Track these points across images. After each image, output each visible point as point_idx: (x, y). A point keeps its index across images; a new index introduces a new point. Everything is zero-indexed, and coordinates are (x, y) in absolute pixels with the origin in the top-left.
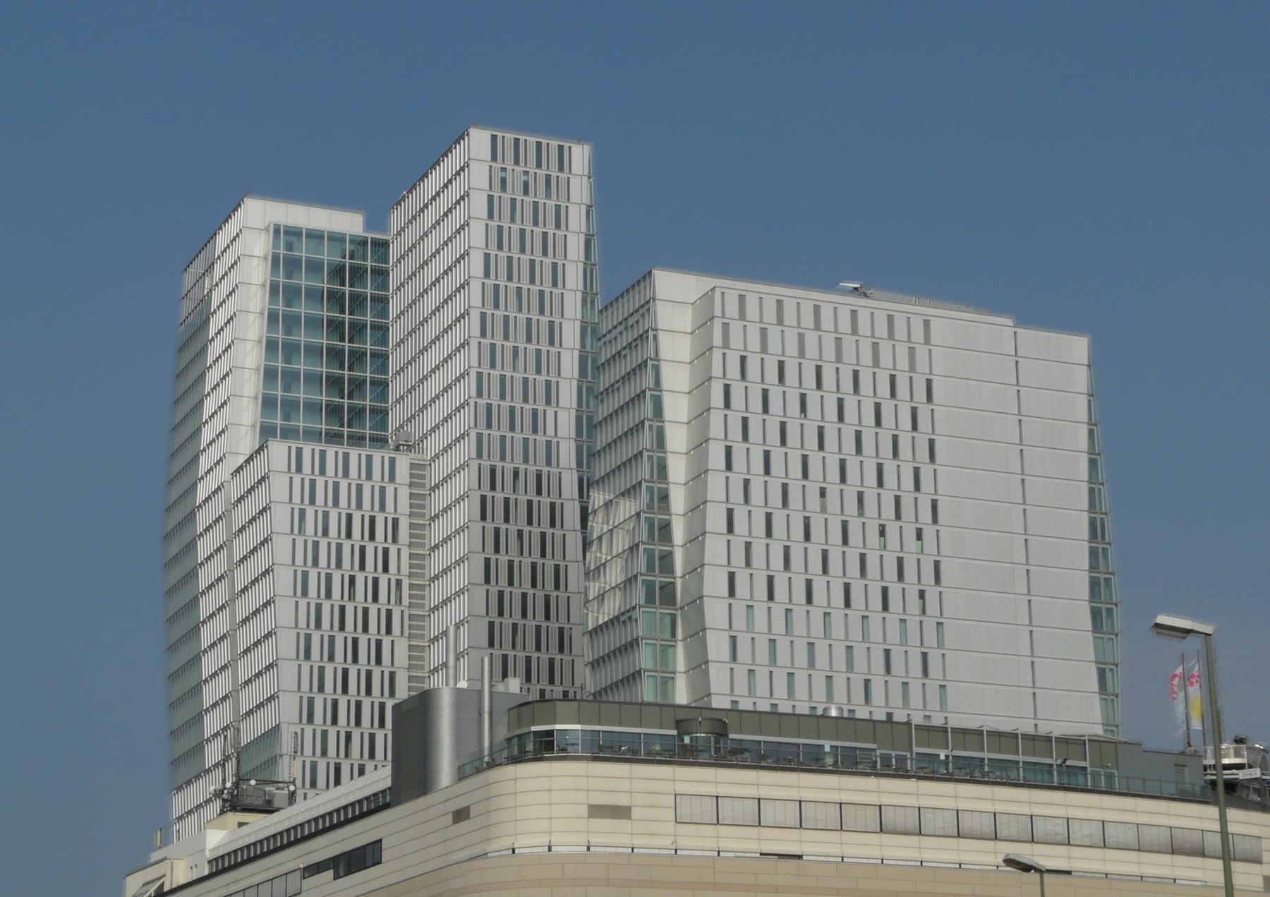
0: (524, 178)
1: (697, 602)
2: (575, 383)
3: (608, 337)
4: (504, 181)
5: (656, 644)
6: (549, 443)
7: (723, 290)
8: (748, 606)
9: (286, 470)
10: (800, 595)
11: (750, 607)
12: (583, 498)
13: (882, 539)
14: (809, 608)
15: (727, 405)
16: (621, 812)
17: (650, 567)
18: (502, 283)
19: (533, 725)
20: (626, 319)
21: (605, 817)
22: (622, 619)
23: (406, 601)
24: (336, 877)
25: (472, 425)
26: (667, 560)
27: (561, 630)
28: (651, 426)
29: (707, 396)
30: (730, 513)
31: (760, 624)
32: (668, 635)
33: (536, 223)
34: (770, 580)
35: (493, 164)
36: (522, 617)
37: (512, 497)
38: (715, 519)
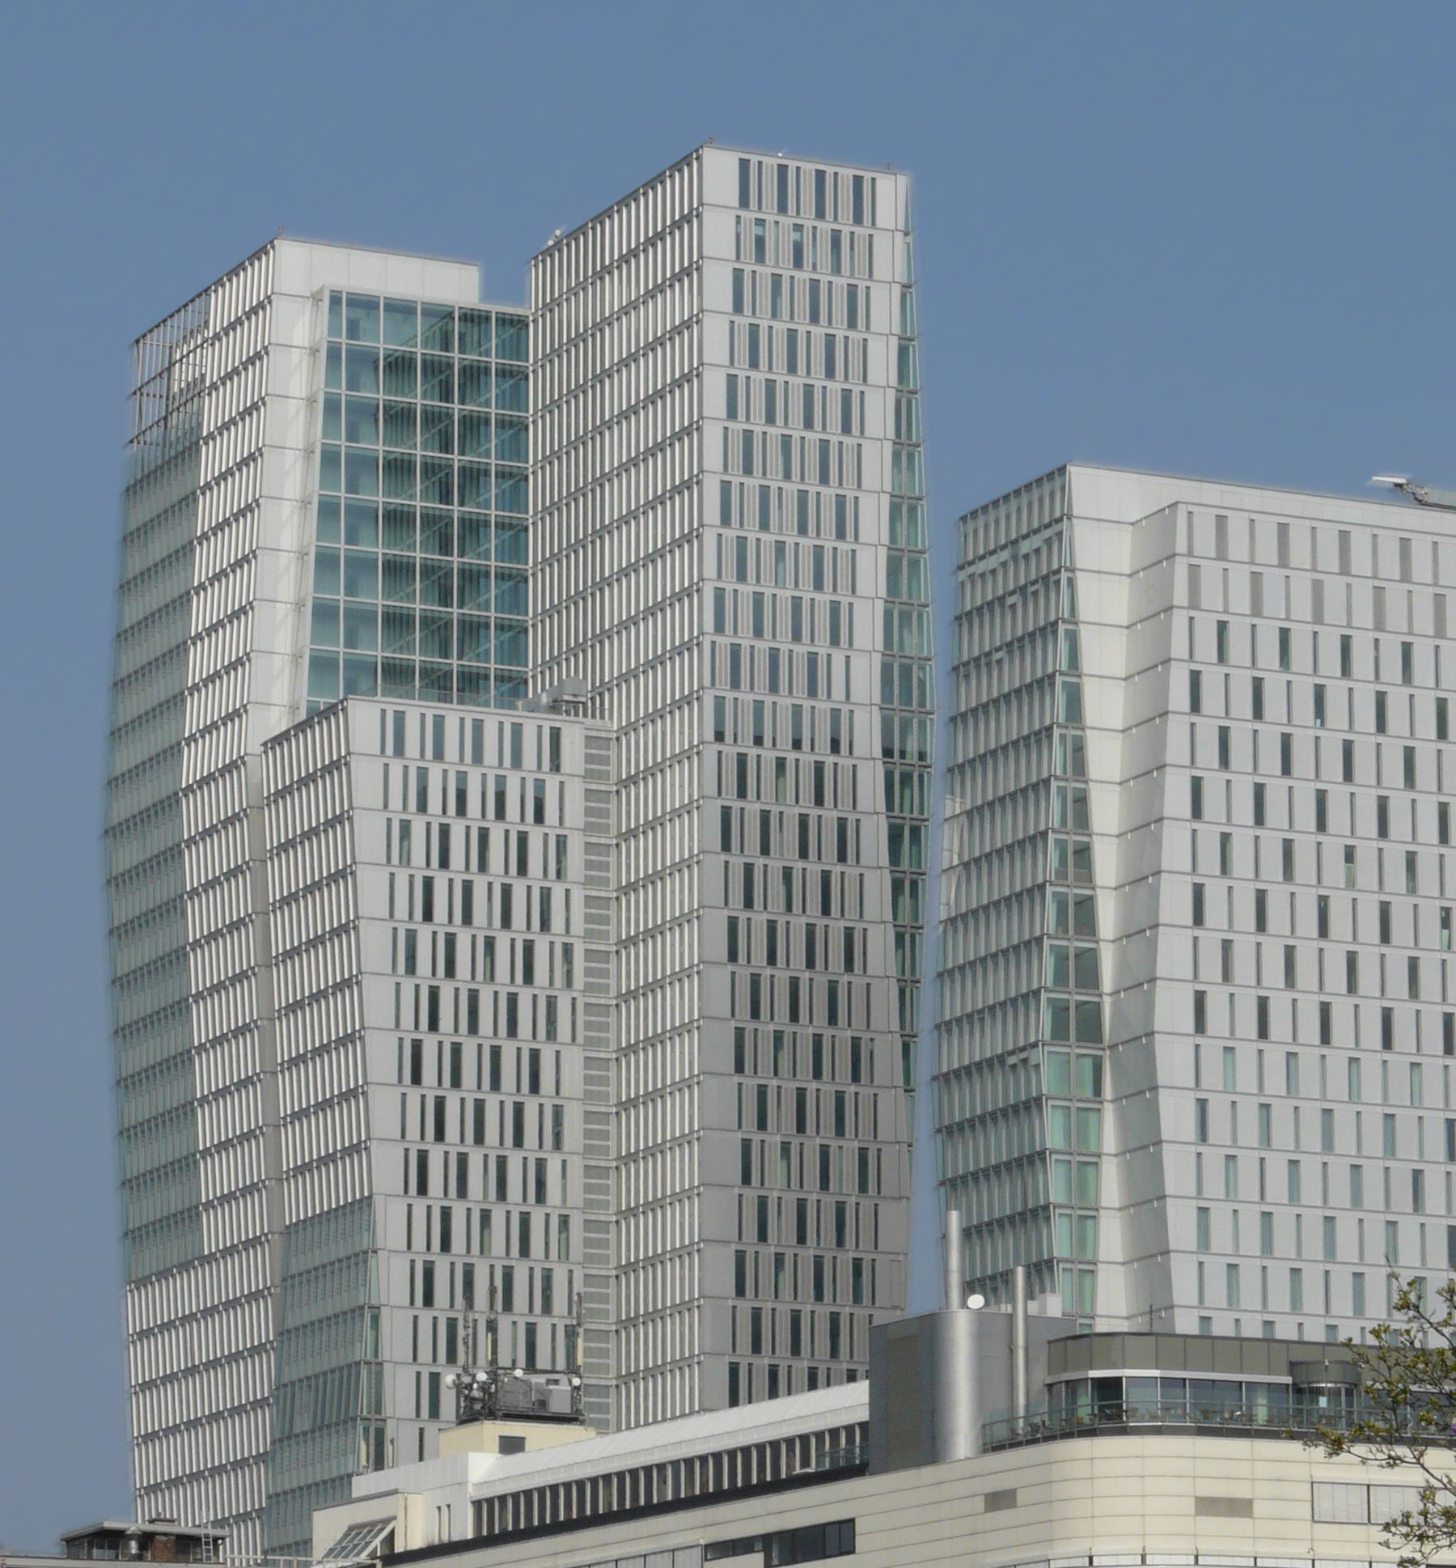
0: (794, 236)
2: (880, 606)
3: (981, 567)
4: (760, 242)
5: (1069, 1108)
6: (836, 714)
7: (1191, 508)
8: (1225, 1048)
10: (1310, 1029)
12: (893, 811)
13: (1446, 932)
14: (1325, 1051)
15: (1195, 706)
16: (1239, 1507)
17: (1061, 977)
18: (758, 428)
20: (1015, 542)
21: (1218, 1514)
22: (1012, 1060)
23: (579, 980)
25: (707, 682)
26: (1088, 973)
28: (1063, 737)
29: (1162, 690)
30: (1198, 892)
32: (1088, 1092)
34: (1263, 1005)
35: (743, 214)
36: (791, 1021)
37: (775, 810)
38: (1175, 902)
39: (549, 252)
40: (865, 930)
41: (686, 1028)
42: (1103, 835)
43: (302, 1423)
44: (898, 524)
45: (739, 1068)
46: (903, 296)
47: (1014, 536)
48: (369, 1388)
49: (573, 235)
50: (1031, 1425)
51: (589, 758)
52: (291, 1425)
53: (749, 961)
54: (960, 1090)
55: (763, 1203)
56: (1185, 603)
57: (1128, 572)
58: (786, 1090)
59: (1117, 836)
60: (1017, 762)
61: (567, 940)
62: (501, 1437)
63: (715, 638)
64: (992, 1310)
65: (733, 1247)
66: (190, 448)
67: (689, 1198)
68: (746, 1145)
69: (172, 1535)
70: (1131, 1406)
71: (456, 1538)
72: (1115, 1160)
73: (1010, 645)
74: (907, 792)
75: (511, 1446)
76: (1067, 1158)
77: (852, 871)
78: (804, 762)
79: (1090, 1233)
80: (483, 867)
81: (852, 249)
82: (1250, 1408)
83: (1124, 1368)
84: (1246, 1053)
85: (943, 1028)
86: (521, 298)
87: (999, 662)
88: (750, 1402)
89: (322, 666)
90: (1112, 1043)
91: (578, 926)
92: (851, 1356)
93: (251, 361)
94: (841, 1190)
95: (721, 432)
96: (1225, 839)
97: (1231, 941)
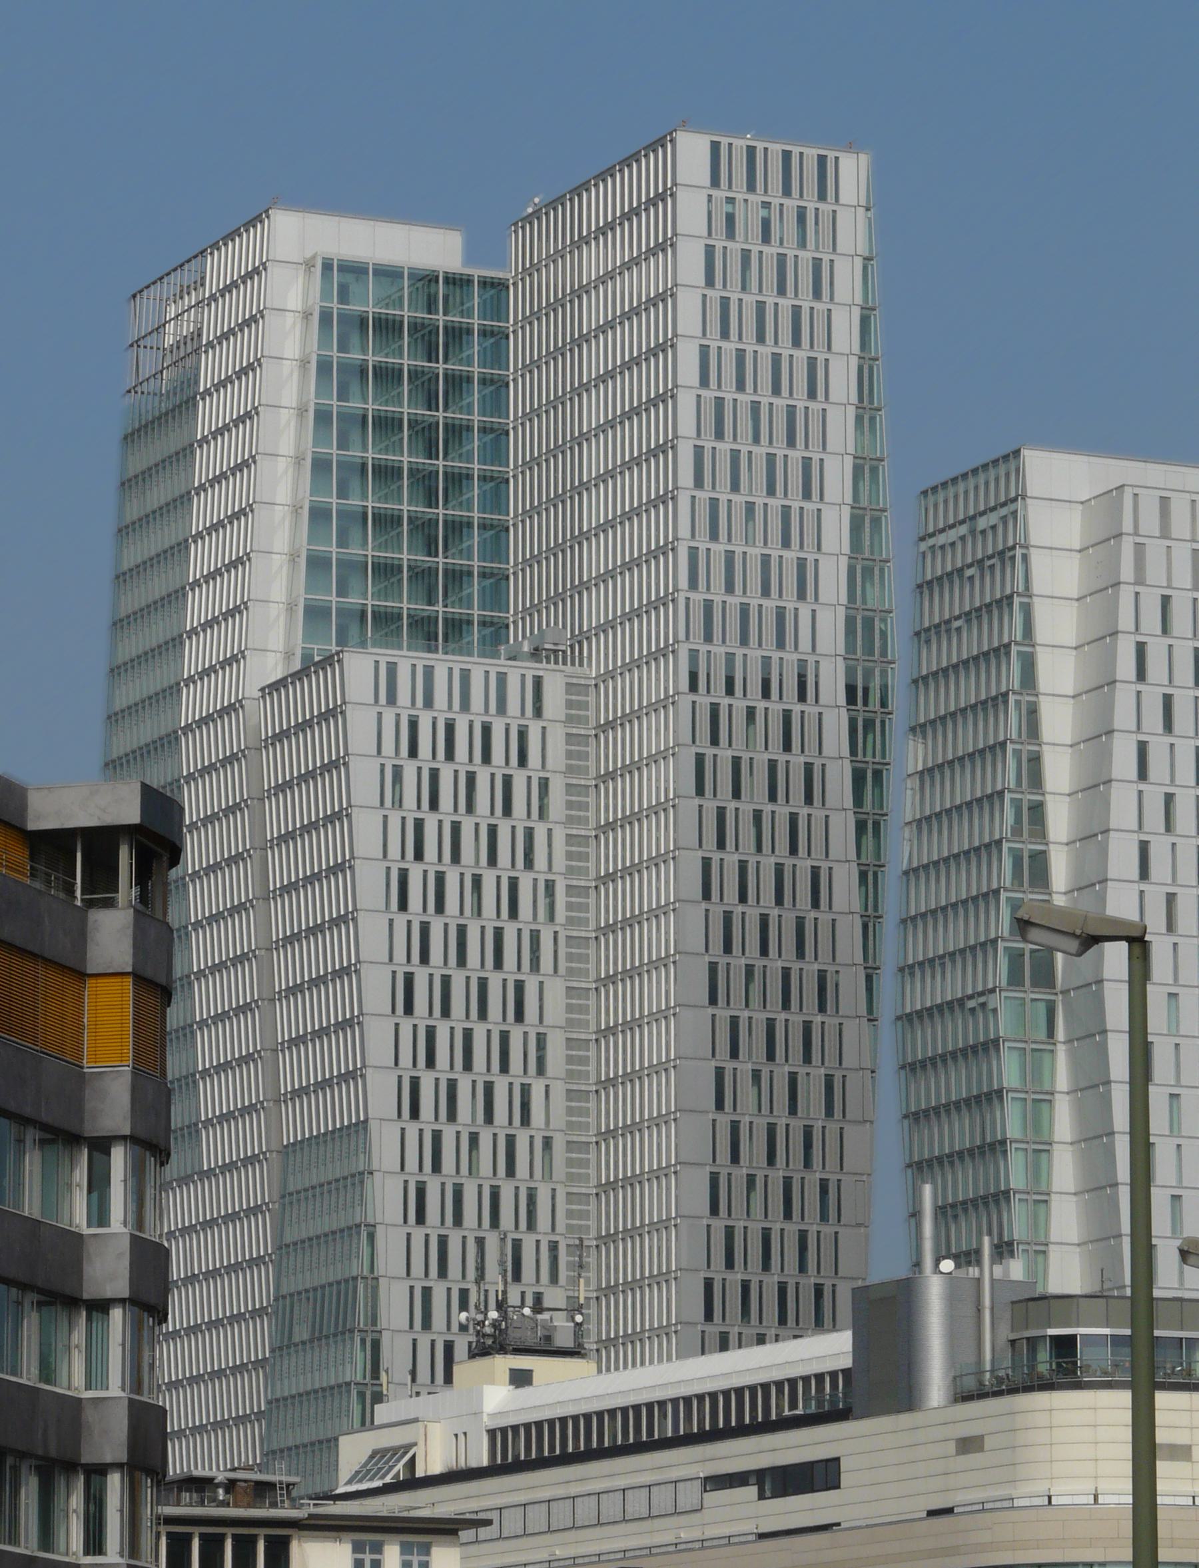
0: (763, 213)
2: (844, 562)
3: (941, 539)
4: (730, 219)
5: (1025, 1049)
6: (802, 663)
7: (1136, 491)
8: (1170, 994)
9: (372, 701)
11: (1173, 996)
12: (856, 755)
15: (1141, 675)
19: (1050, 1327)
20: (973, 518)
22: (971, 1004)
23: (561, 913)
24: (762, 1497)
25: (682, 636)
27: (822, 976)
28: (1018, 703)
30: (1144, 848)
32: (1042, 1034)
33: (782, 291)
35: (715, 193)
37: (745, 756)
39: (528, 219)
40: (830, 868)
41: (661, 963)
42: (1054, 794)
43: (301, 1333)
44: (861, 484)
45: (713, 1001)
46: (865, 268)
47: (971, 513)
48: (366, 1297)
49: (552, 204)
50: (997, 1378)
51: (570, 704)
52: (291, 1333)
53: (722, 899)
54: (922, 1030)
55: (735, 1127)
57: (1078, 548)
58: (757, 1020)
59: (1069, 795)
60: (975, 724)
61: (550, 877)
62: (511, 1370)
63: (690, 595)
64: (961, 1273)
65: (708, 1169)
66: (187, 402)
67: (666, 1122)
68: (720, 1073)
69: (251, 1481)
70: (1085, 1363)
71: (473, 1464)
72: (1067, 1098)
73: (968, 614)
74: (870, 737)
75: (521, 1379)
76: (1023, 1096)
77: (818, 814)
78: (773, 710)
79: (1045, 1115)
80: (470, 808)
81: (817, 223)
82: (1189, 1364)
83: (1078, 1326)
85: (907, 970)
86: (503, 264)
87: (959, 629)
88: (740, 1347)
89: (315, 614)
90: (1066, 988)
91: (560, 863)
92: (819, 1272)
93: (247, 323)
94: (808, 1114)
95: (694, 399)
96: (1169, 799)
97: (1175, 894)
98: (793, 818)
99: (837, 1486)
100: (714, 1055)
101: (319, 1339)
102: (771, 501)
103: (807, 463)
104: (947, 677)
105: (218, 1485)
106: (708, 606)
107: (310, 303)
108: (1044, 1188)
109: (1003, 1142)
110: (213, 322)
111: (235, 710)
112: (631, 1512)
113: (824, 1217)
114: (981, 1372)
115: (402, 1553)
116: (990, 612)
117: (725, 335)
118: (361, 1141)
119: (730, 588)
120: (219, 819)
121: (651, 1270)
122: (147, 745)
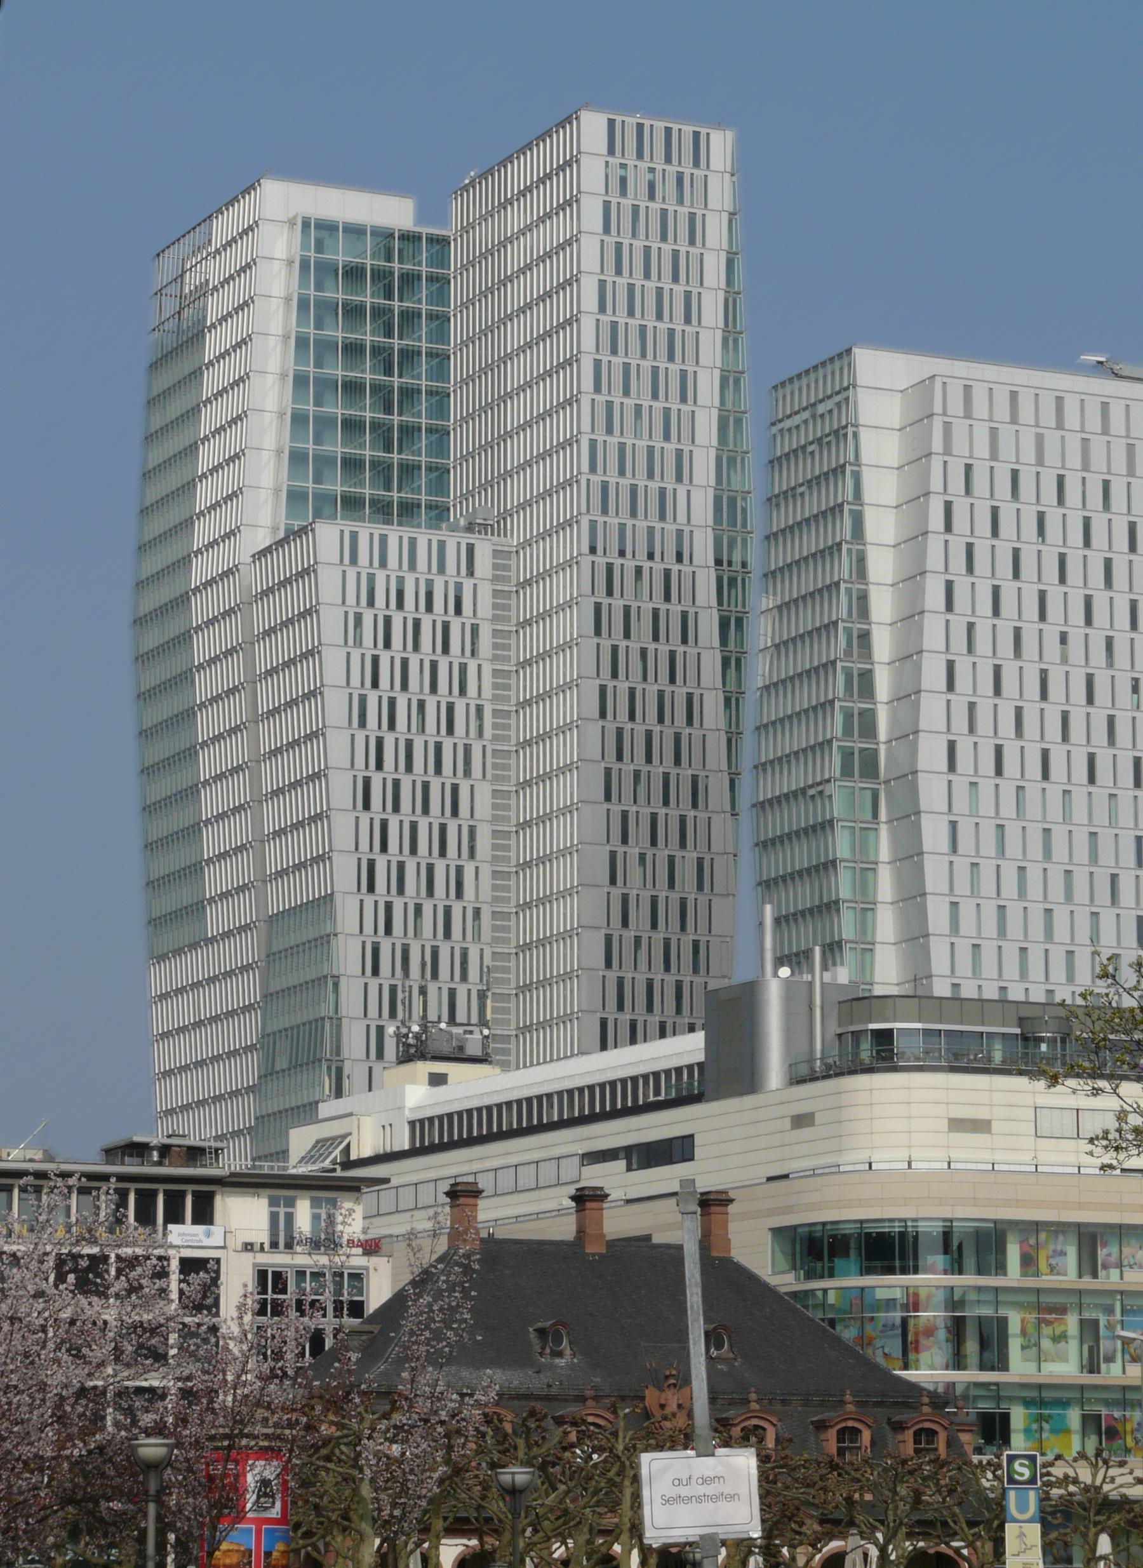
0: (649, 176)
1: (909, 777)
2: (713, 453)
3: (788, 424)
4: (623, 181)
7: (945, 380)
8: (971, 783)
11: (973, 784)
13: (1135, 696)
15: (948, 527)
16: (981, 1126)
20: (814, 405)
21: (965, 1131)
22: (811, 792)
23: (488, 732)
25: (584, 509)
26: (868, 727)
28: (849, 551)
31: (987, 806)
37: (634, 605)
38: (933, 674)
39: (465, 188)
43: (281, 1063)
45: (608, 798)
46: (730, 221)
47: (813, 400)
49: (483, 176)
50: (826, 1065)
51: (495, 567)
55: (625, 899)
56: (941, 451)
60: (815, 569)
63: (590, 477)
64: (797, 978)
65: (603, 932)
66: (197, 335)
68: (613, 855)
71: (396, 1148)
72: (888, 866)
73: (809, 482)
74: (733, 592)
75: (437, 1080)
76: (853, 905)
80: (416, 647)
81: (692, 186)
82: (989, 1052)
83: (895, 1021)
84: (986, 787)
86: (445, 223)
87: (802, 494)
89: (296, 497)
90: (887, 778)
92: (692, 1013)
93: (243, 270)
95: (594, 322)
96: (971, 627)
98: (672, 654)
99: (691, 1158)
100: (608, 841)
101: (295, 1067)
102: (655, 404)
103: (683, 374)
104: (792, 533)
105: (153, 1148)
106: (605, 486)
107: (293, 252)
108: (869, 939)
109: (837, 902)
110: (214, 270)
111: (233, 573)
112: (521, 1185)
113: (696, 970)
114: (811, 1060)
115: (312, 1207)
116: (827, 480)
117: (619, 272)
118: (329, 909)
119: (622, 472)
120: (220, 660)
121: (558, 1012)
122: (166, 605)
